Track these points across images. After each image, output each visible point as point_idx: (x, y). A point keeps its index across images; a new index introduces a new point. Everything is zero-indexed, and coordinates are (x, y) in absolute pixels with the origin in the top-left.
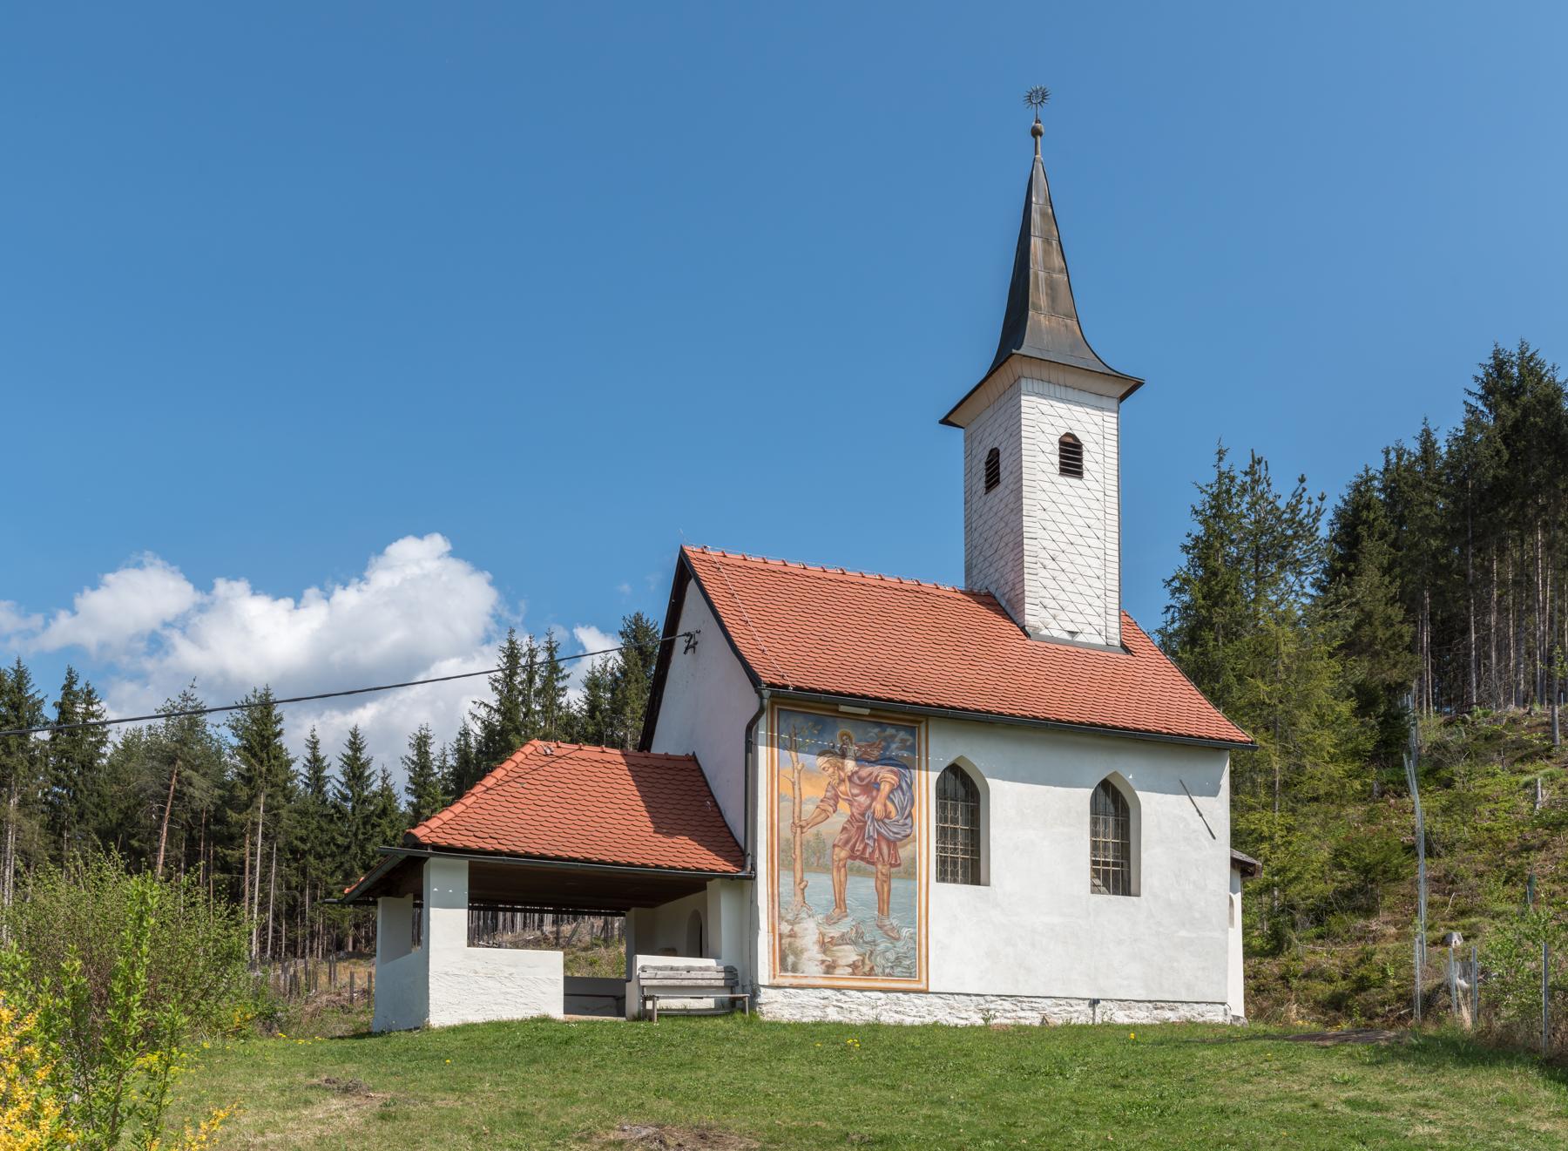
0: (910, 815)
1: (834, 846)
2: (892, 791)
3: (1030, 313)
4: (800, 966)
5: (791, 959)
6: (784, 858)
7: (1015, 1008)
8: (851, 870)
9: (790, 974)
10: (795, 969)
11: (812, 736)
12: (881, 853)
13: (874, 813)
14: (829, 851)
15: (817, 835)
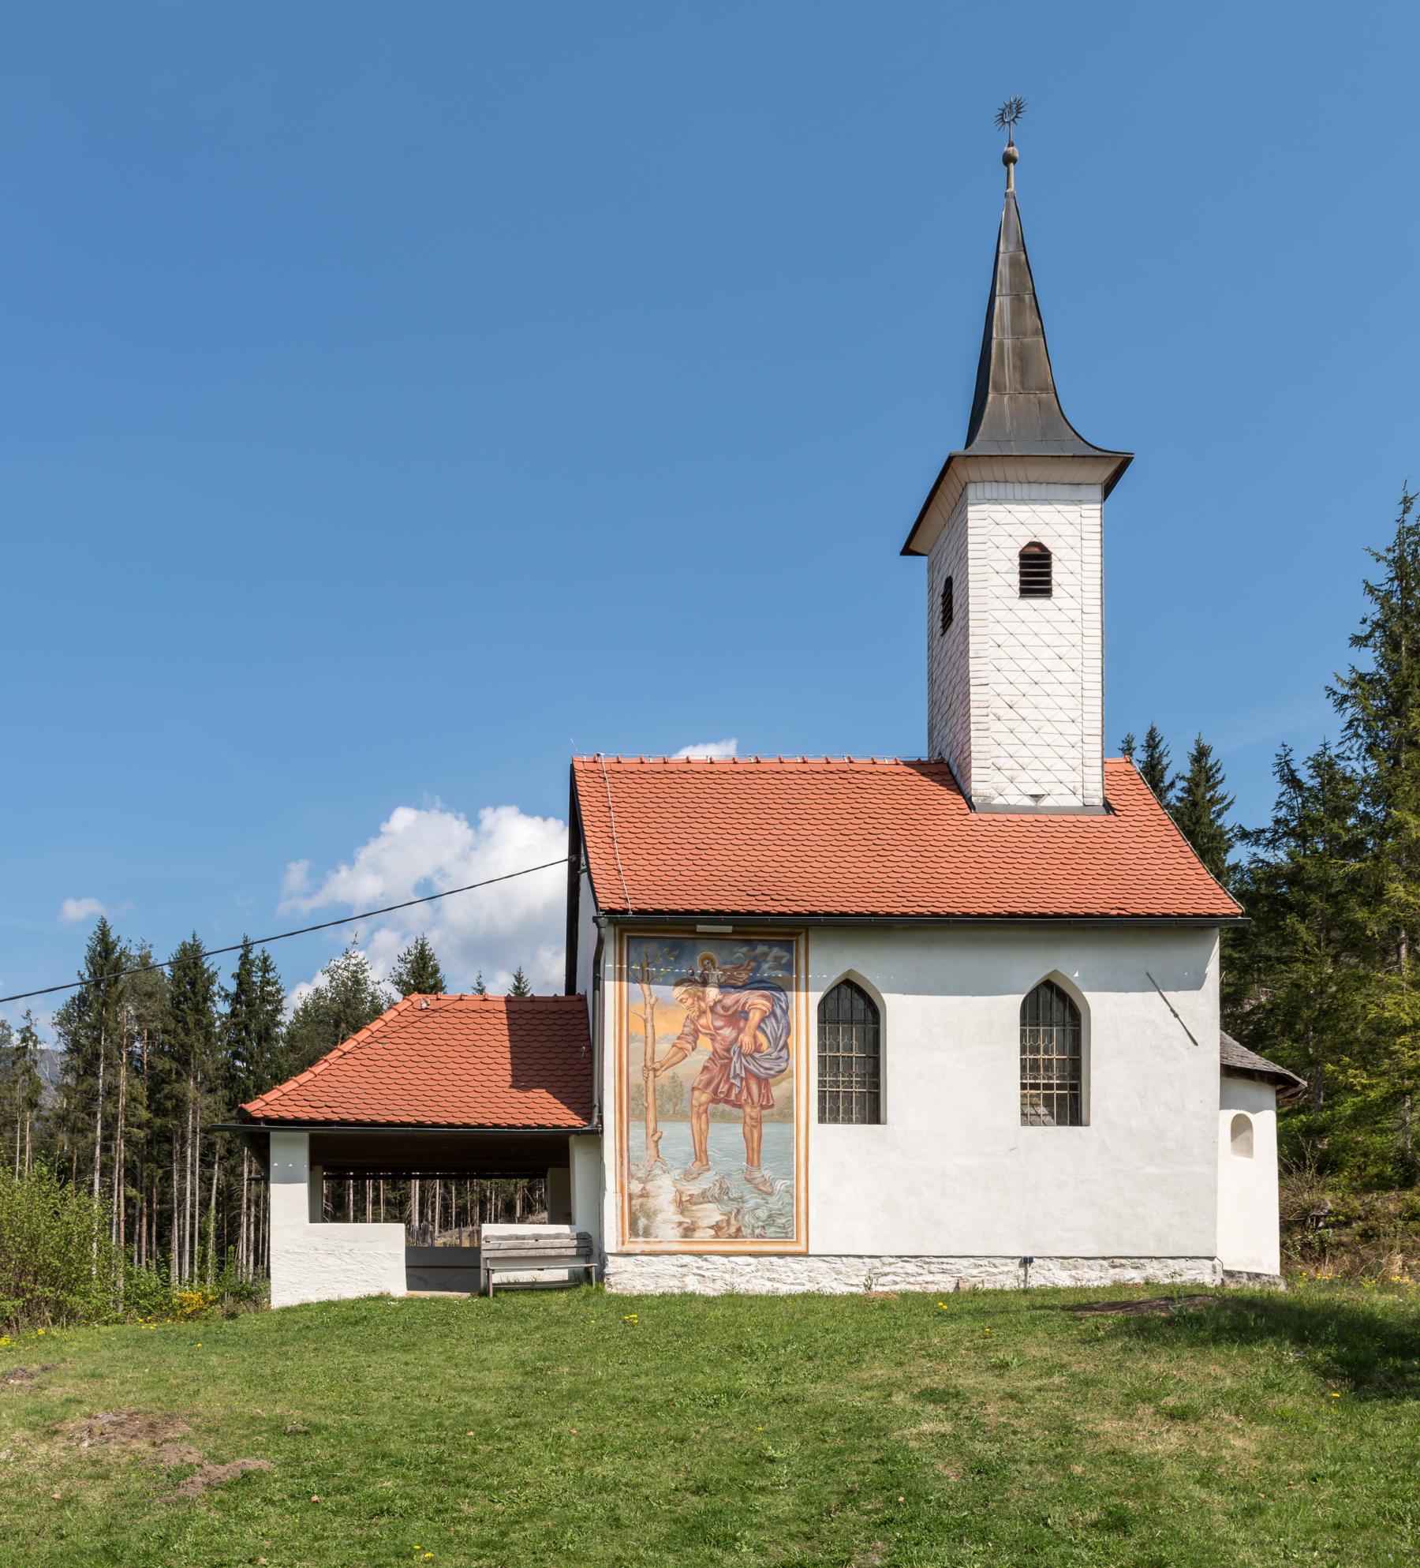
0: (786, 1045)
1: (693, 1089)
2: (763, 1020)
3: (990, 397)
4: (653, 1230)
5: (642, 1222)
6: (634, 1107)
7: (920, 1271)
8: (714, 1115)
9: (641, 1239)
10: (647, 1233)
11: (667, 964)
12: (749, 1094)
13: (741, 1047)
14: (687, 1096)
15: (673, 1078)
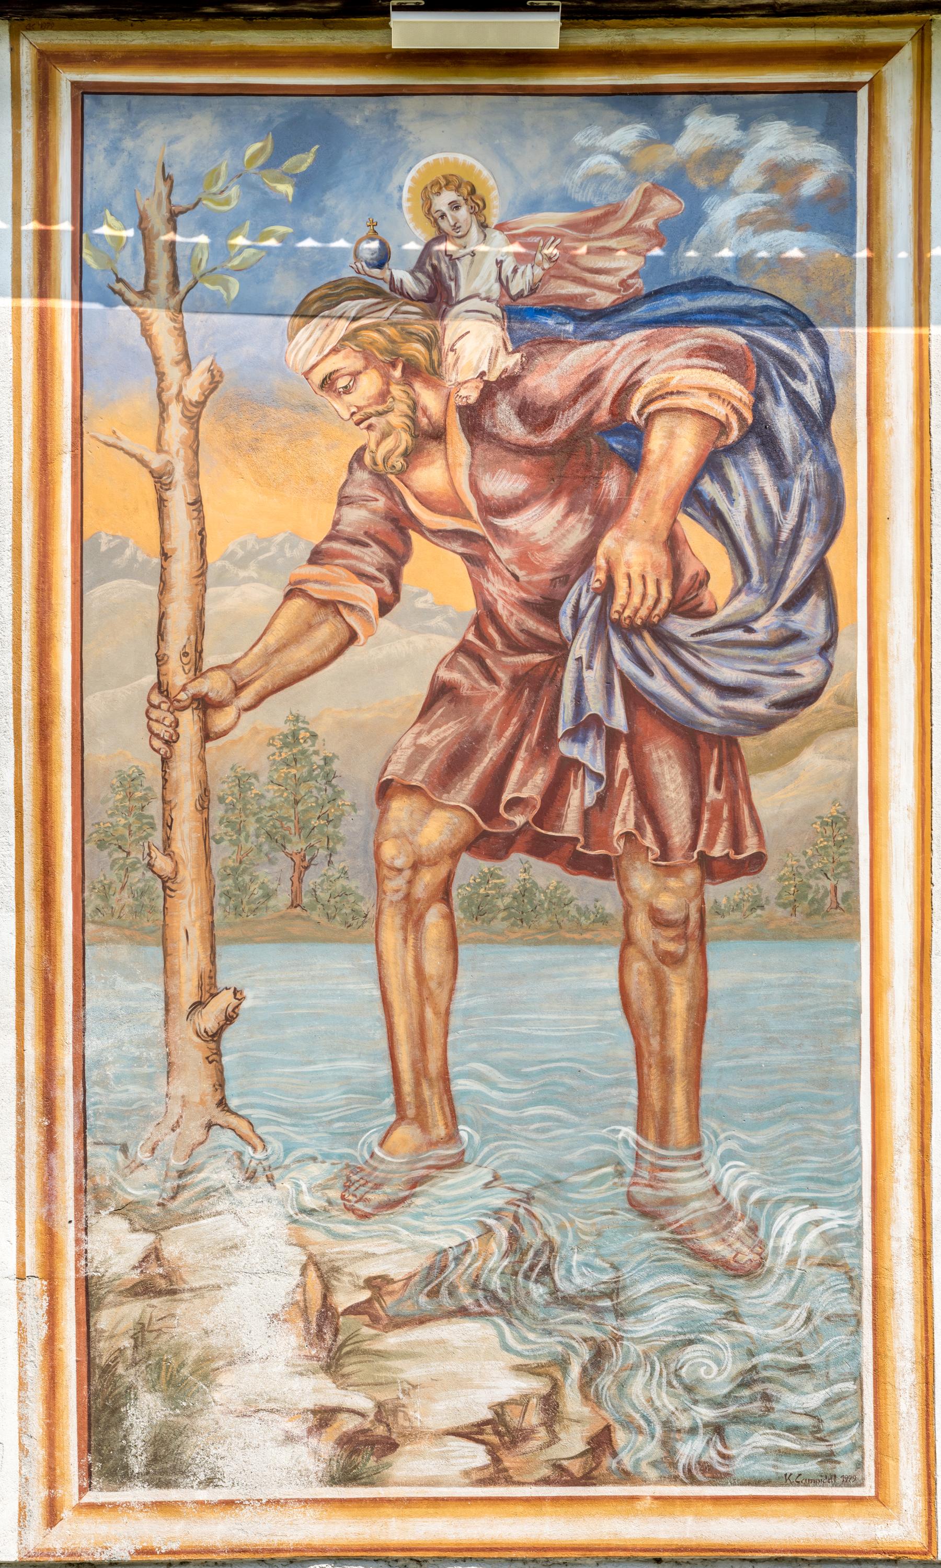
13: (608, 590)
